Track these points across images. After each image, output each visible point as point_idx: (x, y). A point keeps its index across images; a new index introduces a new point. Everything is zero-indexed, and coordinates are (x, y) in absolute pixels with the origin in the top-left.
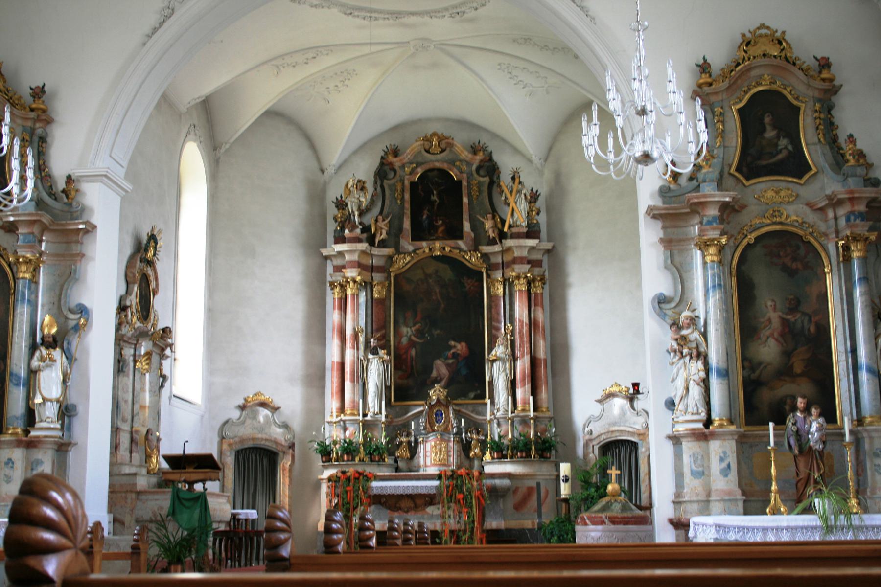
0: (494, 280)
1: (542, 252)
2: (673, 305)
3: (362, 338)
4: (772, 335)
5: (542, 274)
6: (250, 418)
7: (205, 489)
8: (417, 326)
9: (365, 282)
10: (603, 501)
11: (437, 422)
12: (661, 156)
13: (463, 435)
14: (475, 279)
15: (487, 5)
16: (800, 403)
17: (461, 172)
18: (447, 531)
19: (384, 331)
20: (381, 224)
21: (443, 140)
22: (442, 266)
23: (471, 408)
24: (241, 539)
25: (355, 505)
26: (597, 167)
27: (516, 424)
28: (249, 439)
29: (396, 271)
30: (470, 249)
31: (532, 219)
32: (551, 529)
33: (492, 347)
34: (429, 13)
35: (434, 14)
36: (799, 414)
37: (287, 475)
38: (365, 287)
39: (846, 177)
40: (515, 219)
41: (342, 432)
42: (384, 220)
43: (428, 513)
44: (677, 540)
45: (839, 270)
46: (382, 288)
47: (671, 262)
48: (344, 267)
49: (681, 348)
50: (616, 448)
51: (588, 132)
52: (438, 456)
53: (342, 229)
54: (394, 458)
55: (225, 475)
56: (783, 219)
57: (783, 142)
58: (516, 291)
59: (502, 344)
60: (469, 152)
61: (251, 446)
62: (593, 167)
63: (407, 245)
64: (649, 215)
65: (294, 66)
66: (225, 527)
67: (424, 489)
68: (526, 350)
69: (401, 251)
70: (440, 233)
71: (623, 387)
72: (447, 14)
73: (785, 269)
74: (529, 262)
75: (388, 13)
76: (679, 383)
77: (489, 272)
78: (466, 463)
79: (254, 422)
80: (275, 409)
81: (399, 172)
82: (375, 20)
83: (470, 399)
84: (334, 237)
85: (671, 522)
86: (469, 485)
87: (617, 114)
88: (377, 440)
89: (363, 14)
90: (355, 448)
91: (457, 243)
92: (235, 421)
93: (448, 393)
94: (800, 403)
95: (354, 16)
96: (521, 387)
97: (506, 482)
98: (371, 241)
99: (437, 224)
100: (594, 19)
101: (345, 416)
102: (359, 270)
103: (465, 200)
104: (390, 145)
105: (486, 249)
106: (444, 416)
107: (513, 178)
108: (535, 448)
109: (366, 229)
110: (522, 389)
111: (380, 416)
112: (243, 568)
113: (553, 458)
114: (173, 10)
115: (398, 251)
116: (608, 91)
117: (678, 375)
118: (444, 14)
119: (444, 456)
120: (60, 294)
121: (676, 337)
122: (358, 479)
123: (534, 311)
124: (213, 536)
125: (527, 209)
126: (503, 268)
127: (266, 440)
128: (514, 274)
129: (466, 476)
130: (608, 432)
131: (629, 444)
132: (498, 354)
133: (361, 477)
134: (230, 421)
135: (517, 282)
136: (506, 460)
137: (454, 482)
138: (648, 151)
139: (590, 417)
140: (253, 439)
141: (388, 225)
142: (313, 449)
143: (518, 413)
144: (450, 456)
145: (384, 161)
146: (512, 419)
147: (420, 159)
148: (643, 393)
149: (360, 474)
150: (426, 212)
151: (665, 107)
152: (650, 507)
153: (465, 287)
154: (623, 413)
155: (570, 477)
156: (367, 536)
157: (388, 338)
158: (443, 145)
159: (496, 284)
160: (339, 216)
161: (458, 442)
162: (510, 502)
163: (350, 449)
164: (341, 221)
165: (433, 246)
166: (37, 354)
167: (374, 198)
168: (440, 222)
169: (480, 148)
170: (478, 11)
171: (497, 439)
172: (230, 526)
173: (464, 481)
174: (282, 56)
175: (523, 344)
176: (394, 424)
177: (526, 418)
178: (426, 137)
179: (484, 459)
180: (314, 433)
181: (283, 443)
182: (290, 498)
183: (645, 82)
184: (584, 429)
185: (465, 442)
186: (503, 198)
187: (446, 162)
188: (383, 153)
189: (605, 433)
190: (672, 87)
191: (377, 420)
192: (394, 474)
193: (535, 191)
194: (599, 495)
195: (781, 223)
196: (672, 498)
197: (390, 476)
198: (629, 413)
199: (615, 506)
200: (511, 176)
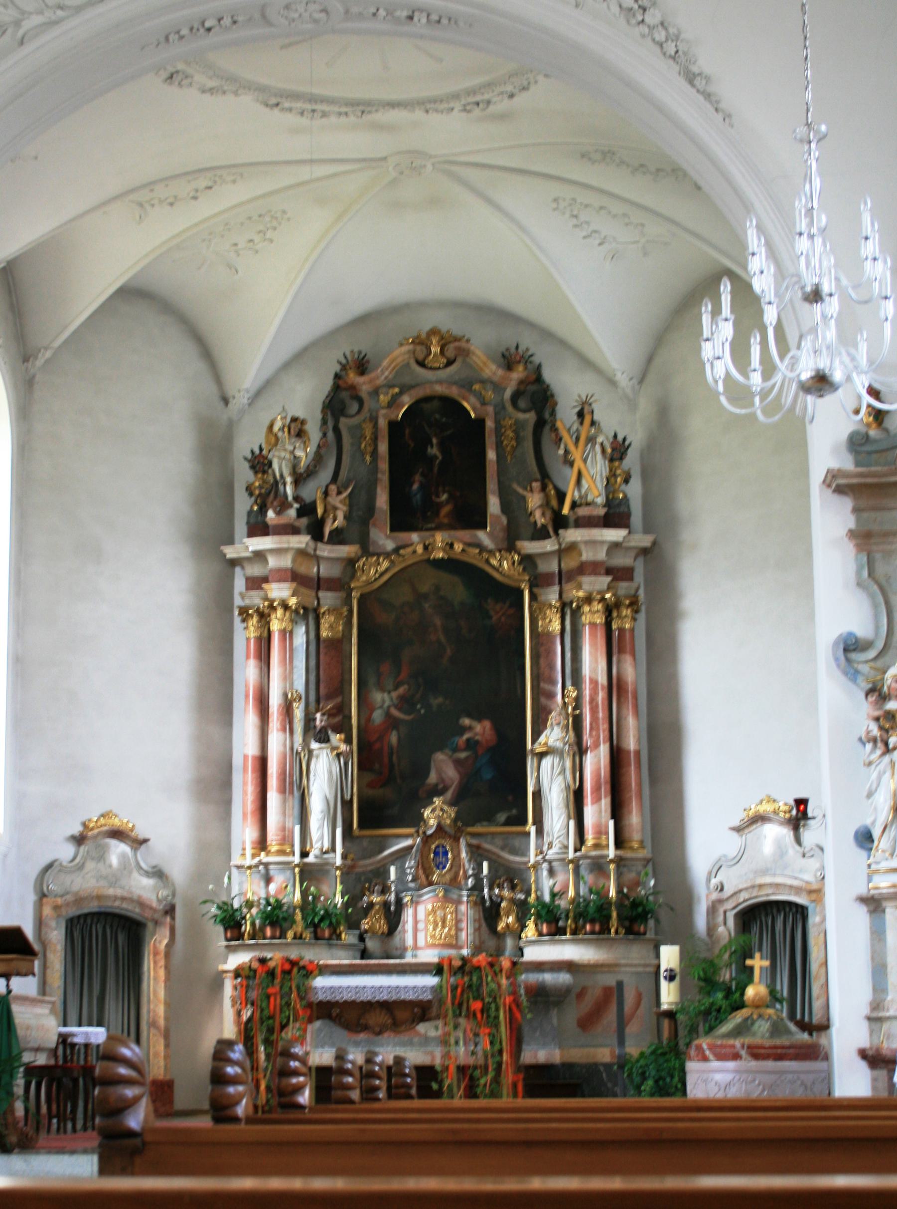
0: (544, 605)
1: (633, 554)
2: (872, 654)
3: (299, 713)
5: (633, 592)
6: (93, 859)
7: (9, 992)
8: (401, 690)
9: (305, 608)
10: (738, 1017)
11: (438, 868)
12: (849, 379)
13: (486, 891)
14: (507, 604)
15: (533, 88)
17: (484, 403)
18: (453, 1069)
19: (339, 699)
20: (335, 500)
21: (450, 342)
22: (446, 578)
24: (75, 1081)
25: (285, 1021)
26: (731, 400)
27: (583, 871)
28: (92, 898)
29: (361, 587)
30: (500, 547)
31: (614, 492)
32: (641, 1067)
34: (423, 103)
35: (432, 106)
37: (162, 963)
38: (305, 617)
40: (583, 491)
41: (262, 884)
42: (339, 493)
43: (418, 1034)
44: (874, 1088)
46: (337, 619)
47: (870, 575)
48: (266, 580)
49: (885, 736)
50: (767, 915)
51: (712, 334)
52: (438, 930)
53: (263, 509)
54: (357, 932)
55: (48, 964)
58: (584, 625)
59: (558, 724)
60: (499, 366)
61: (96, 910)
62: (723, 399)
63: (383, 538)
64: (829, 486)
65: (171, 204)
66: (48, 1058)
67: (411, 992)
68: (603, 735)
69: (371, 549)
70: (444, 516)
71: (781, 804)
72: (457, 106)
74: (609, 571)
75: (346, 105)
76: (882, 799)
77: (535, 590)
78: (491, 943)
79: (101, 865)
80: (139, 843)
81: (368, 404)
82: (322, 117)
83: (497, 825)
84: (248, 523)
85: (863, 1054)
86: (493, 986)
87: (767, 300)
88: (326, 899)
89: (299, 105)
90: (285, 915)
91: (476, 536)
92: (65, 864)
93: (458, 814)
95: (283, 110)
96: (593, 803)
97: (564, 978)
98: (316, 531)
99: (438, 500)
100: (730, 116)
101: (267, 854)
102: (294, 585)
103: (491, 455)
104: (352, 352)
105: (530, 547)
106: (450, 856)
107: (581, 415)
108: (618, 915)
109: (306, 510)
110: (596, 807)
111: (331, 855)
112: (80, 1134)
113: (650, 935)
115: (367, 550)
116: (750, 257)
117: (878, 785)
118: (452, 105)
119: (450, 929)
121: (877, 713)
122: (289, 972)
123: (619, 662)
124: (24, 1077)
125: (606, 472)
126: (560, 583)
127: (123, 899)
128: (581, 594)
129: (488, 969)
130: (753, 887)
131: (791, 909)
132: (551, 742)
133: (295, 970)
134: (56, 864)
135: (586, 609)
136: (564, 937)
137: (466, 979)
138: (823, 370)
139: (719, 860)
140: (99, 897)
141: (347, 501)
142: (210, 915)
143: (587, 851)
144: (461, 930)
145: (341, 383)
146: (575, 862)
147: (407, 380)
148: (814, 818)
149: (293, 963)
150: (417, 478)
151: (856, 287)
152: (825, 1027)
153: (490, 617)
154: (781, 852)
155: (678, 970)
156: (294, 1085)
157: (346, 712)
158: (450, 352)
159: (548, 612)
160: (257, 484)
161: (475, 904)
162: (572, 1013)
163: (278, 917)
164: (260, 495)
165: (431, 540)
167: (323, 451)
168: (444, 497)
169: (518, 358)
170: (516, 99)
171: (547, 898)
172: (56, 1057)
173: (484, 978)
174: (150, 185)
175: (598, 725)
176: (358, 870)
177: (603, 861)
178: (418, 337)
179: (523, 935)
180: (211, 887)
181: (154, 904)
182: (167, 1005)
183: (820, 240)
184: (708, 880)
185: (488, 904)
186: (561, 452)
187: (455, 383)
188: (338, 368)
189: (746, 889)
190: (870, 248)
191: (327, 864)
192: (358, 962)
193: (620, 438)
194: (730, 1005)
196: (865, 1010)
197: (350, 966)
198: (791, 852)
199: (760, 1027)
200: (577, 410)
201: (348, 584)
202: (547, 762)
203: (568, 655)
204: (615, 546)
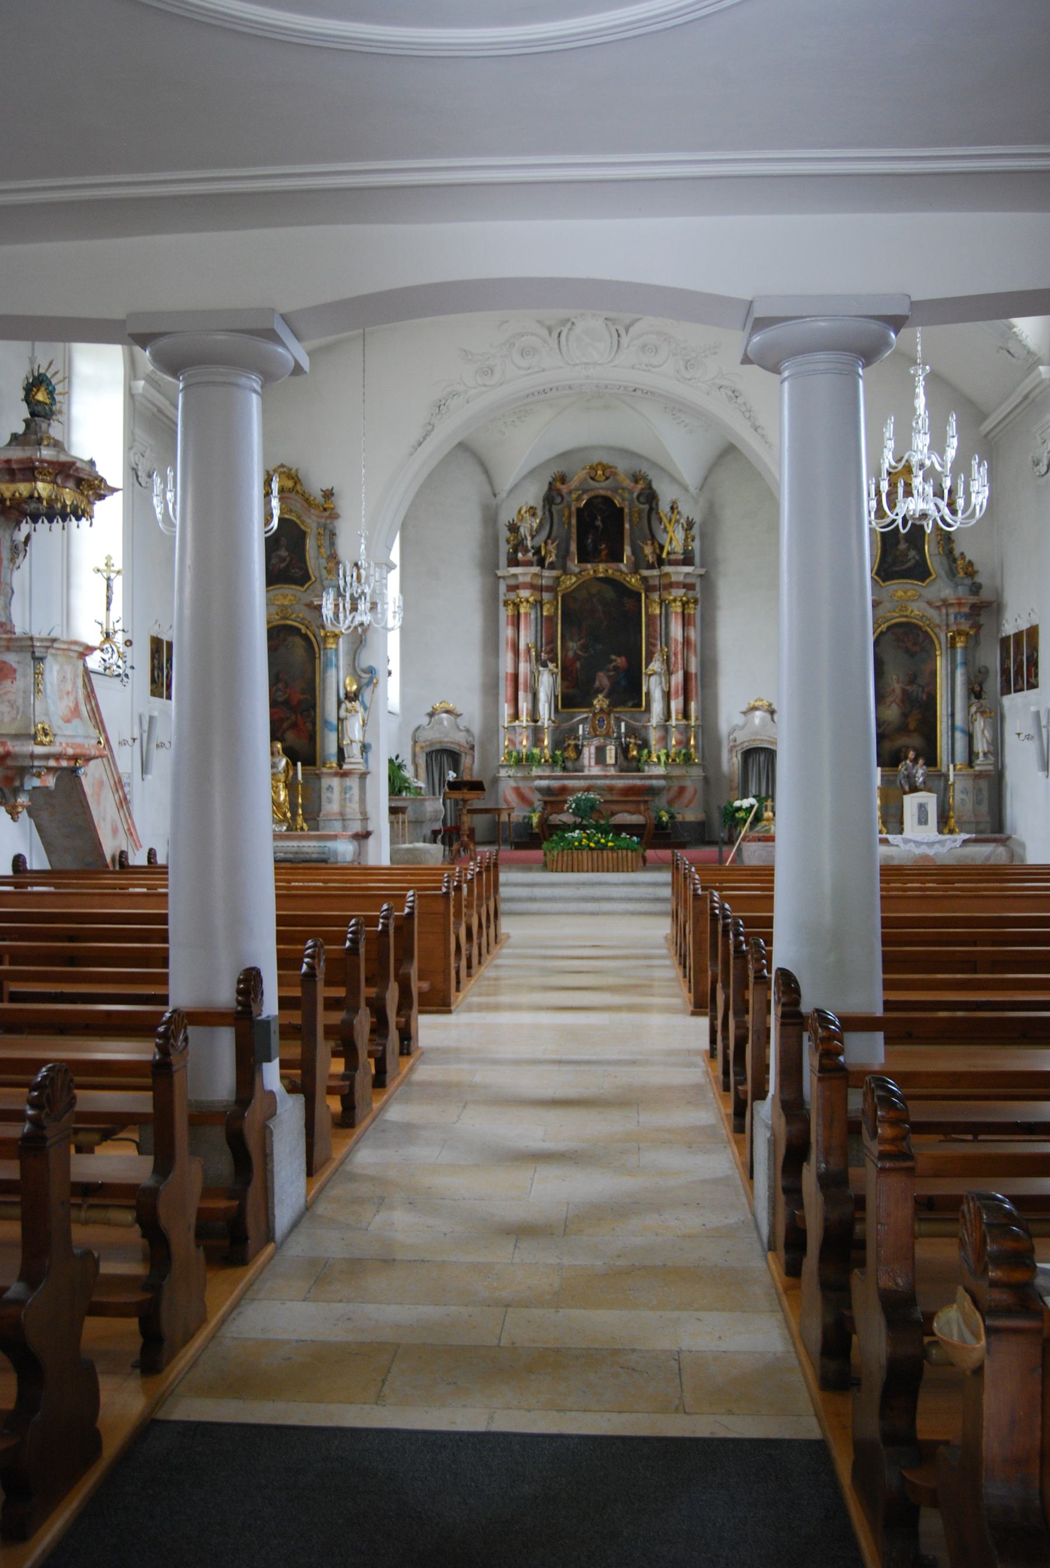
4: (894, 701)
8: (582, 641)
16: (911, 754)
17: (623, 500)
19: (552, 646)
23: (629, 715)
33: (649, 660)
36: (908, 762)
39: (956, 585)
42: (552, 543)
45: (947, 653)
53: (516, 551)
56: (908, 613)
57: (912, 553)
63: (574, 565)
73: (907, 651)
81: (567, 498)
84: (508, 558)
93: (610, 703)
94: (911, 754)
98: (541, 563)
103: (627, 526)
105: (646, 573)
107: (672, 508)
109: (537, 551)
114: (433, 426)
115: (566, 571)
120: (354, 658)
127: (451, 743)
128: (671, 598)
140: (440, 742)
150: (591, 536)
166: (343, 706)
168: (603, 546)
184: (729, 736)
186: (662, 527)
188: (550, 479)
193: (690, 519)
195: (906, 616)
201: (556, 588)
202: (653, 679)
203: (663, 626)
204: (687, 574)
